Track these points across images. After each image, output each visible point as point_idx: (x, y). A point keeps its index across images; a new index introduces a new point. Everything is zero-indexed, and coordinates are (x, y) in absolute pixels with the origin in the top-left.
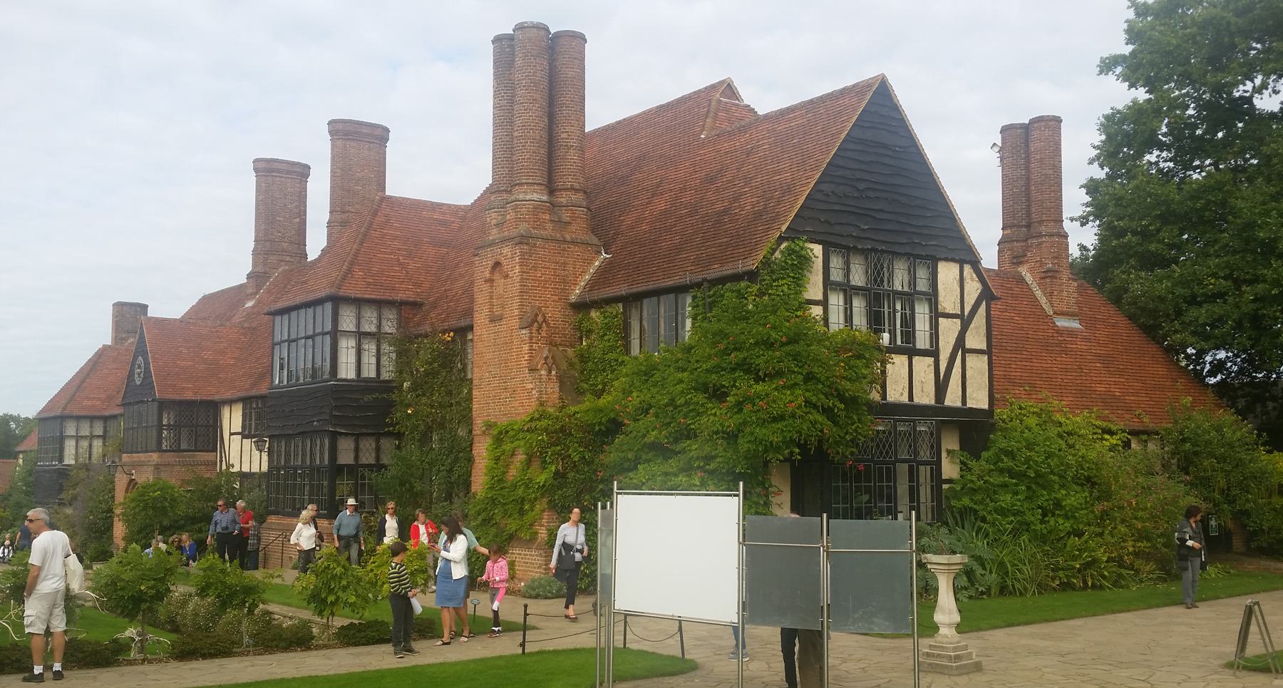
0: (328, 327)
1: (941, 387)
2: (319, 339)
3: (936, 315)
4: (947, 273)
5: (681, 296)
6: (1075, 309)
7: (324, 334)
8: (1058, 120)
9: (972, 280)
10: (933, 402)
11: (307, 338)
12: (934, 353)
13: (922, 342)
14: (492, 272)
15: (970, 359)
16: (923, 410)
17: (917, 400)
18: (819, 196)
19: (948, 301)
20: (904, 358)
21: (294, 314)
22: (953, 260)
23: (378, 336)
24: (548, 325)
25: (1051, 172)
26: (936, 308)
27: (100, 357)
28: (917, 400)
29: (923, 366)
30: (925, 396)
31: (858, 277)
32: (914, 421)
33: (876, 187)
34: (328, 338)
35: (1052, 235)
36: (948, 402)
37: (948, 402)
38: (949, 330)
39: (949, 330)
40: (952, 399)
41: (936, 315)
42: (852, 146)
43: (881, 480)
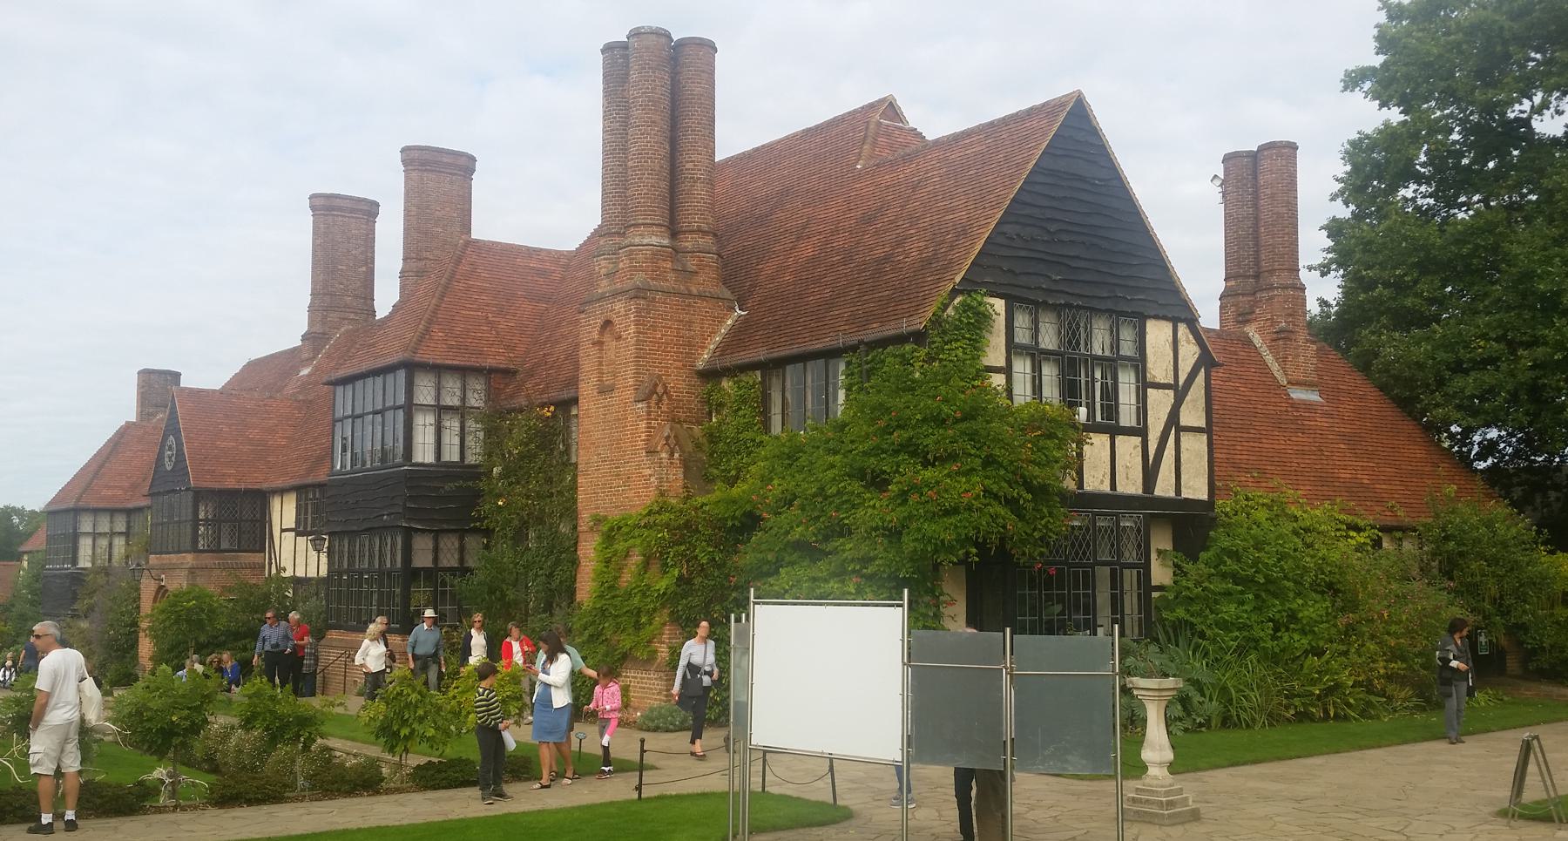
0: (401, 400)
1: (1150, 474)
2: (389, 415)
3: (1144, 385)
4: (1158, 334)
5: (832, 362)
6: (1313, 378)
7: (396, 408)
8: (1293, 147)
9: (1188, 342)
10: (1140, 492)
11: (375, 413)
12: (1141, 431)
13: (1127, 418)
14: (601, 333)
15: (1186, 439)
16: (1128, 501)
17: (1120, 489)
18: (1001, 240)
19: (1159, 369)
20: (1105, 438)
21: (359, 384)
22: (1165, 318)
23: (461, 411)
24: (670, 398)
25: (1284, 210)
26: (1145, 377)
27: (123, 437)
28: (1120, 489)
29: (1128, 447)
30: (1131, 484)
31: (1049, 339)
32: (1117, 515)
33: (1070, 228)
34: (401, 413)
35: (1285, 288)
36: (1158, 492)
37: (1158, 492)
38: (1159, 403)
39: (1159, 403)
40: (1164, 487)
41: (1144, 385)
42: (1041, 179)
43: (1077, 587)
